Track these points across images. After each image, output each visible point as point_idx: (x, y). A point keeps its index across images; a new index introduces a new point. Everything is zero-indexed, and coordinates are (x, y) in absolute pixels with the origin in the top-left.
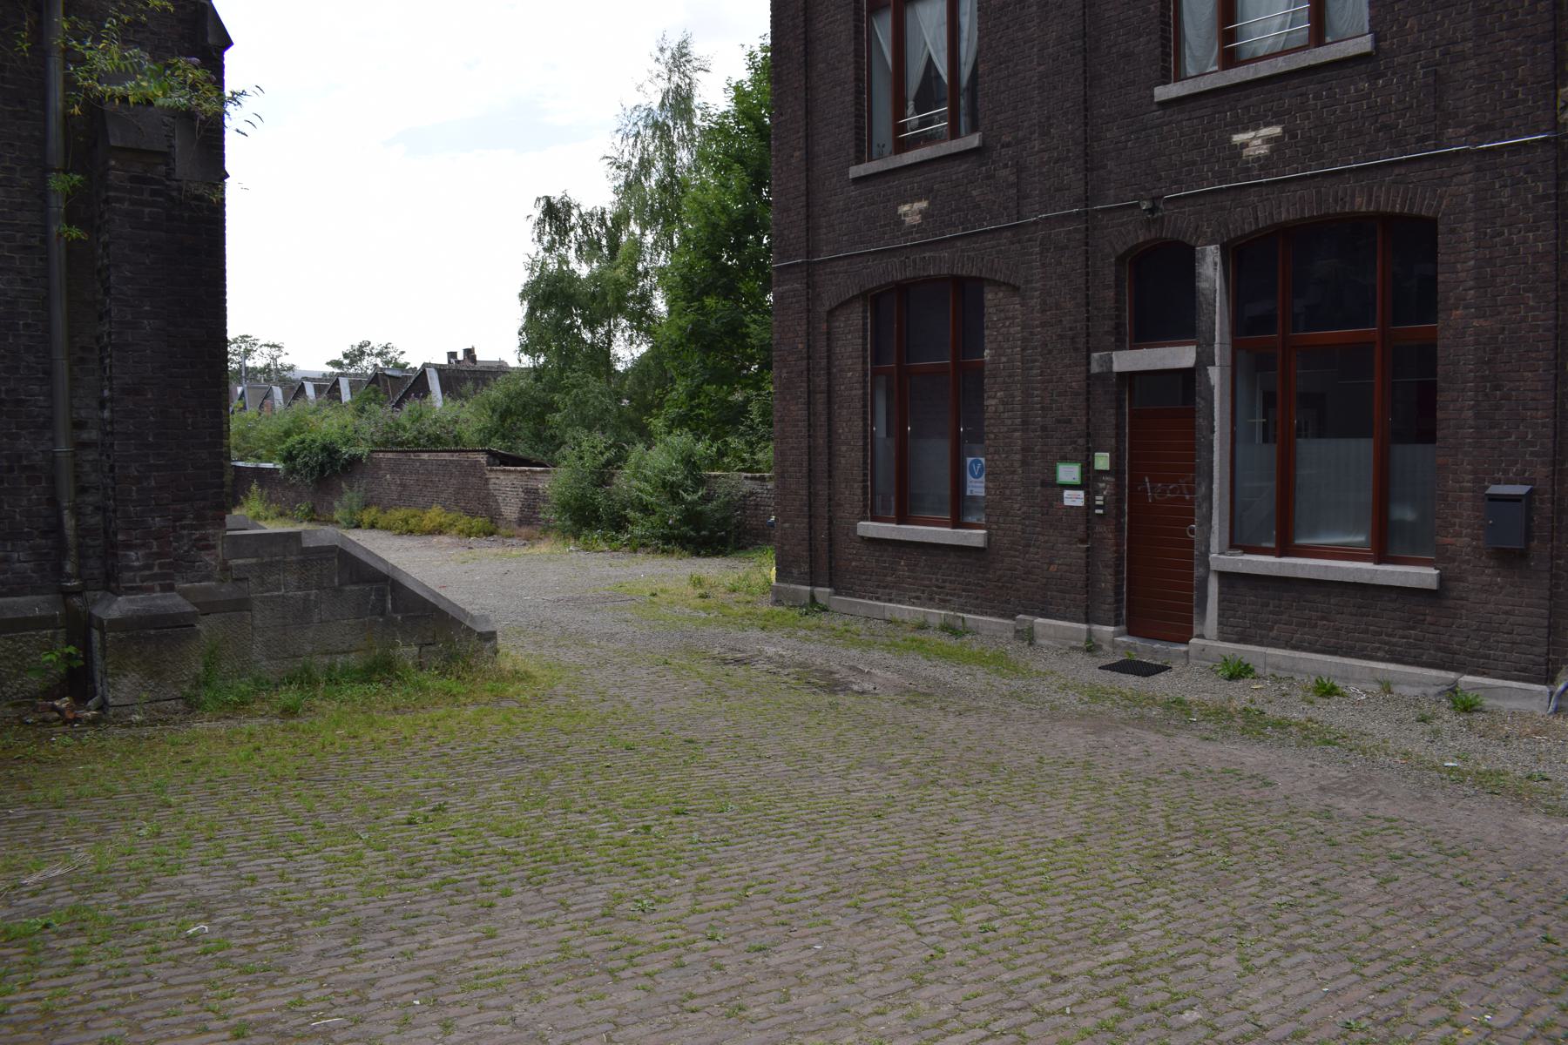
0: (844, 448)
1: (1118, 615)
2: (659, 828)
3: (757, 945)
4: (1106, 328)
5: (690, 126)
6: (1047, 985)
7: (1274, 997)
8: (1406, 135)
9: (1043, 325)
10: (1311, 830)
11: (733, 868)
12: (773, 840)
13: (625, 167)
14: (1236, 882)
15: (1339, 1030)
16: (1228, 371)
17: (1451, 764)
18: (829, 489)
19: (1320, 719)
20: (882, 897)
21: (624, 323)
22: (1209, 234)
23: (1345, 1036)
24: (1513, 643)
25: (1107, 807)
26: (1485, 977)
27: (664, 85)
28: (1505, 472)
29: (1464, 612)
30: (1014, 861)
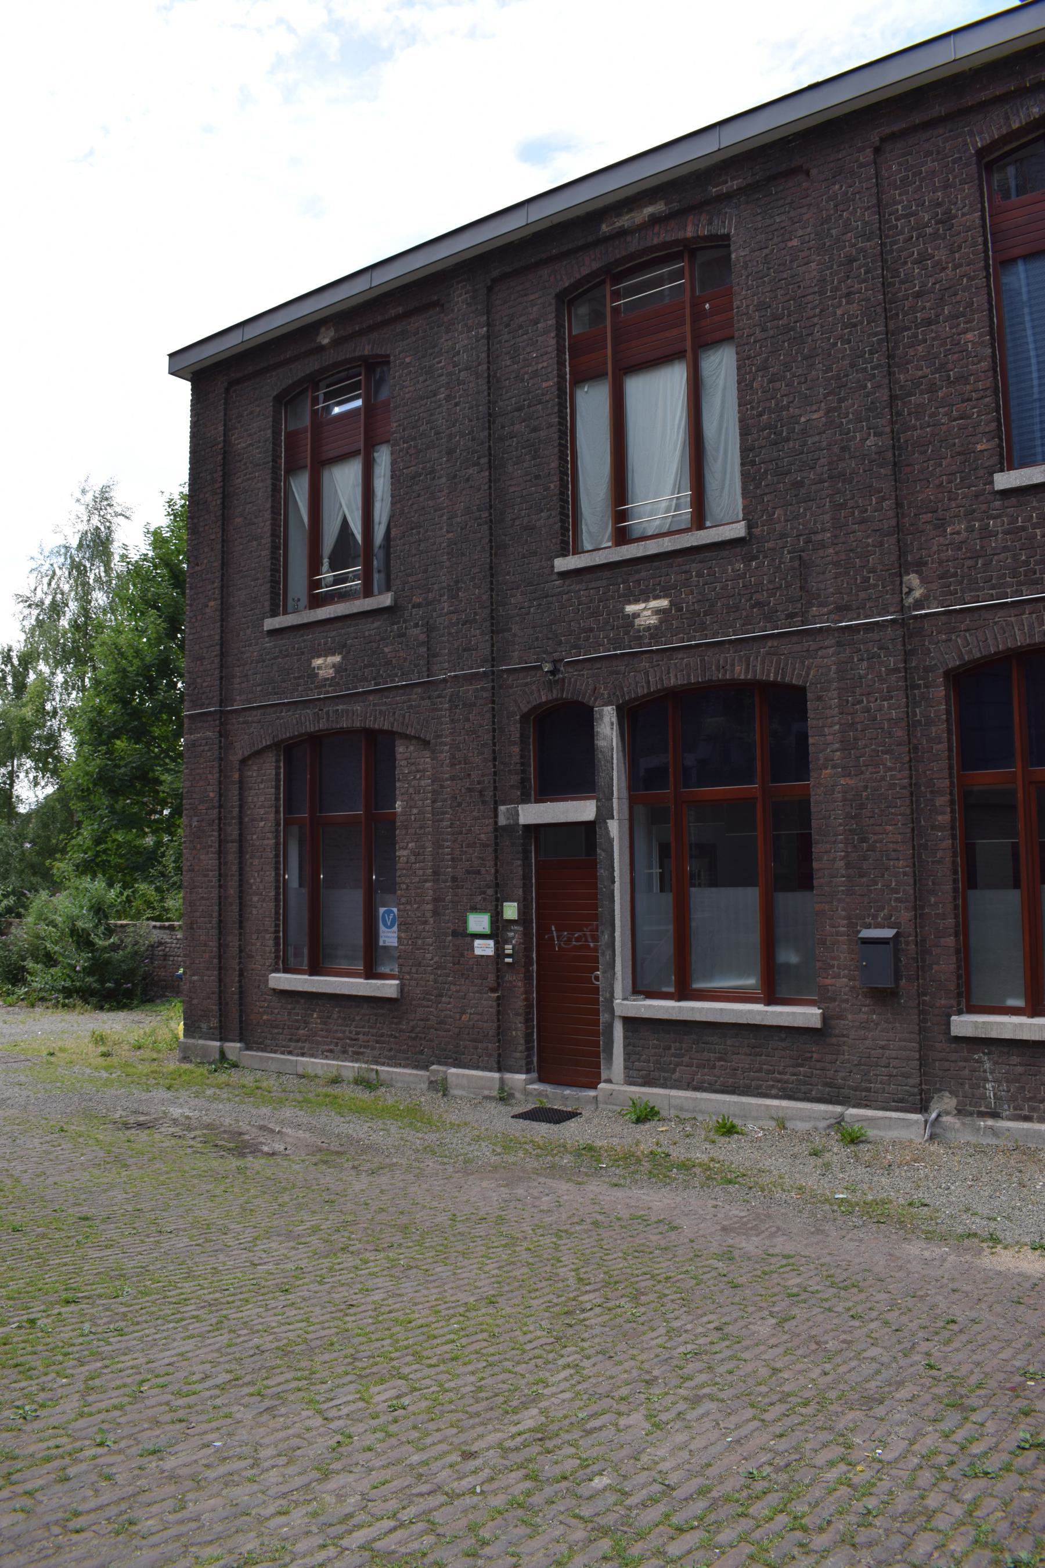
0: (255, 898)
1: (529, 1063)
2: (46, 1321)
3: (151, 1447)
4: (512, 783)
5: (108, 569)
6: (457, 1463)
7: (681, 1453)
8: (777, 611)
9: (452, 778)
10: (714, 1273)
11: (128, 1361)
12: (172, 1325)
13: (37, 605)
14: (644, 1334)
15: (743, 1481)
16: (626, 823)
17: (841, 1196)
18: (240, 940)
19: (721, 1158)
20: (287, 1381)
21: (29, 763)
22: (606, 696)
23: (748, 1487)
24: (890, 1076)
25: (519, 1264)
26: (876, 1410)
27: (83, 527)
28: (875, 917)
29: (846, 1048)
30: (425, 1330)
